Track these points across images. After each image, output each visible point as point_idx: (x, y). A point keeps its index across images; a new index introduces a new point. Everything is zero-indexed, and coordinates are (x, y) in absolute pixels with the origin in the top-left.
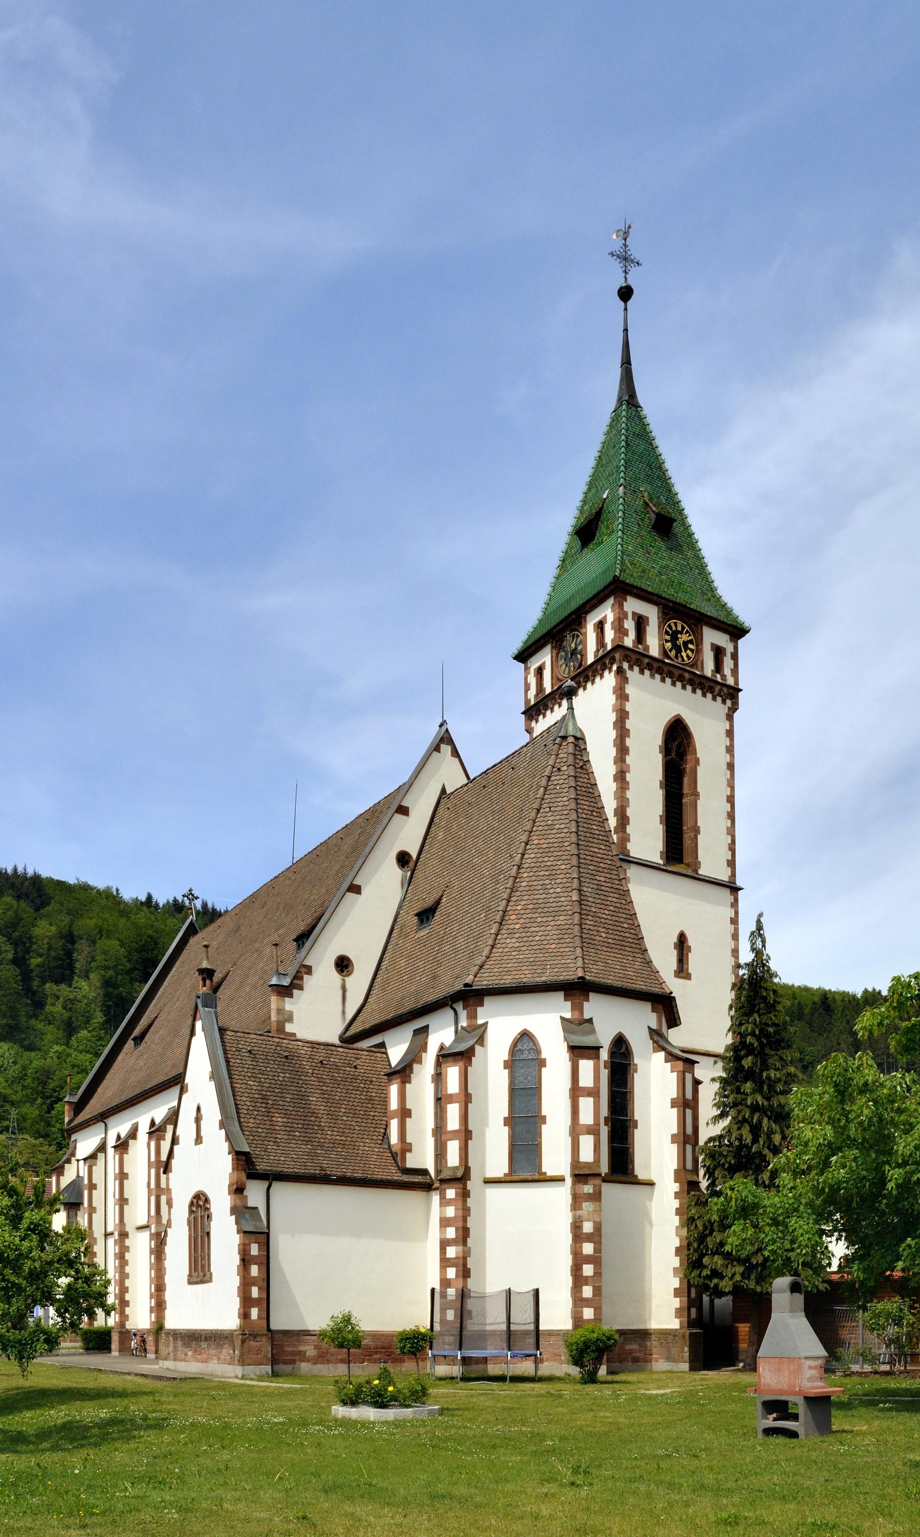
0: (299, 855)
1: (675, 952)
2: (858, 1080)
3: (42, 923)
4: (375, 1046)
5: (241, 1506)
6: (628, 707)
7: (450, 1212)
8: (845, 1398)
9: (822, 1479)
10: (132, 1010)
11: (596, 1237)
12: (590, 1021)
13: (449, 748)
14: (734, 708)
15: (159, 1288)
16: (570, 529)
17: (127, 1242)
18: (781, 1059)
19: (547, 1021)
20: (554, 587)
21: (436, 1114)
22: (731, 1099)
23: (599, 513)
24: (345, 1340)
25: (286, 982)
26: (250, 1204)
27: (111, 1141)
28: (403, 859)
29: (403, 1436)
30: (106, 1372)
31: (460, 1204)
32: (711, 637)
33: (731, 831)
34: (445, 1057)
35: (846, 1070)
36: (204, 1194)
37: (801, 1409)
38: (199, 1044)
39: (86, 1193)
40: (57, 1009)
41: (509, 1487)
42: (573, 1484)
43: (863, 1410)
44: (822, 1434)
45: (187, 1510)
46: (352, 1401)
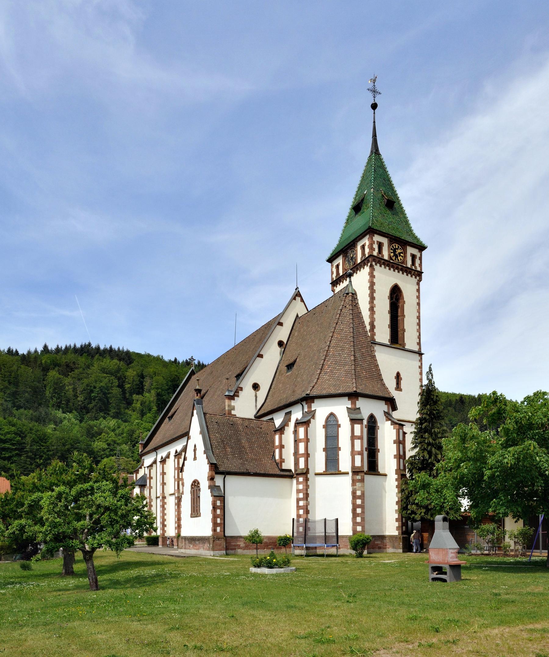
0: (238, 342)
1: (395, 380)
2: (470, 434)
3: (130, 370)
4: (269, 420)
5: (207, 612)
6: (375, 280)
7: (301, 487)
8: (468, 565)
9: (455, 600)
10: (168, 406)
11: (362, 497)
12: (359, 408)
14: (420, 280)
15: (179, 519)
16: (351, 207)
17: (166, 501)
18: (440, 424)
19: (341, 409)
20: (344, 231)
21: (295, 447)
22: (419, 441)
23: (363, 200)
24: (255, 540)
25: (232, 394)
26: (216, 485)
27: (159, 459)
28: (280, 344)
29: (279, 580)
30: (156, 554)
31: (305, 484)
32: (410, 250)
33: (419, 331)
34: (298, 423)
35: (465, 430)
36: (197, 481)
37: (448, 570)
38: (195, 421)
39: (148, 481)
40: (138, 405)
41: (321, 603)
42: (348, 601)
43: (475, 571)
44: (457, 581)
45: (184, 613)
46: (258, 566)
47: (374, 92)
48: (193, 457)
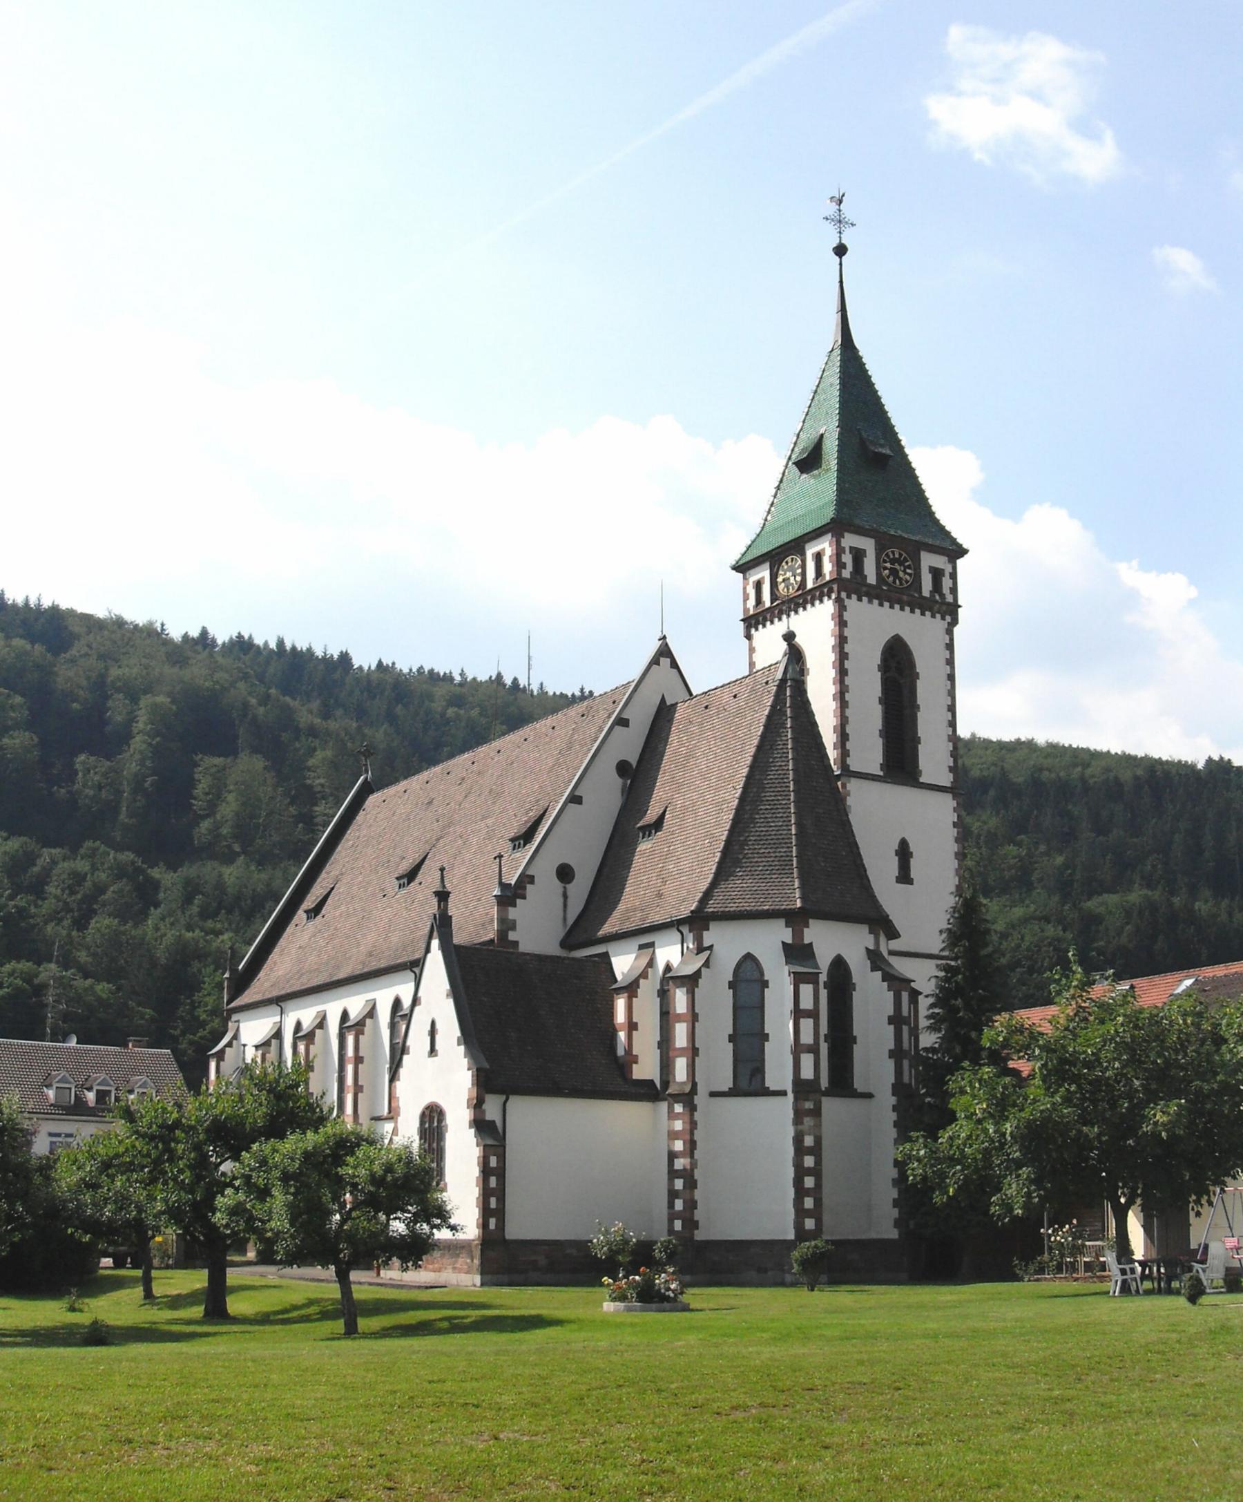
7: (678, 1125)
11: (816, 1151)
13: (668, 660)
14: (955, 622)
19: (766, 942)
31: (687, 1118)
32: (929, 560)
48: (428, 1048)
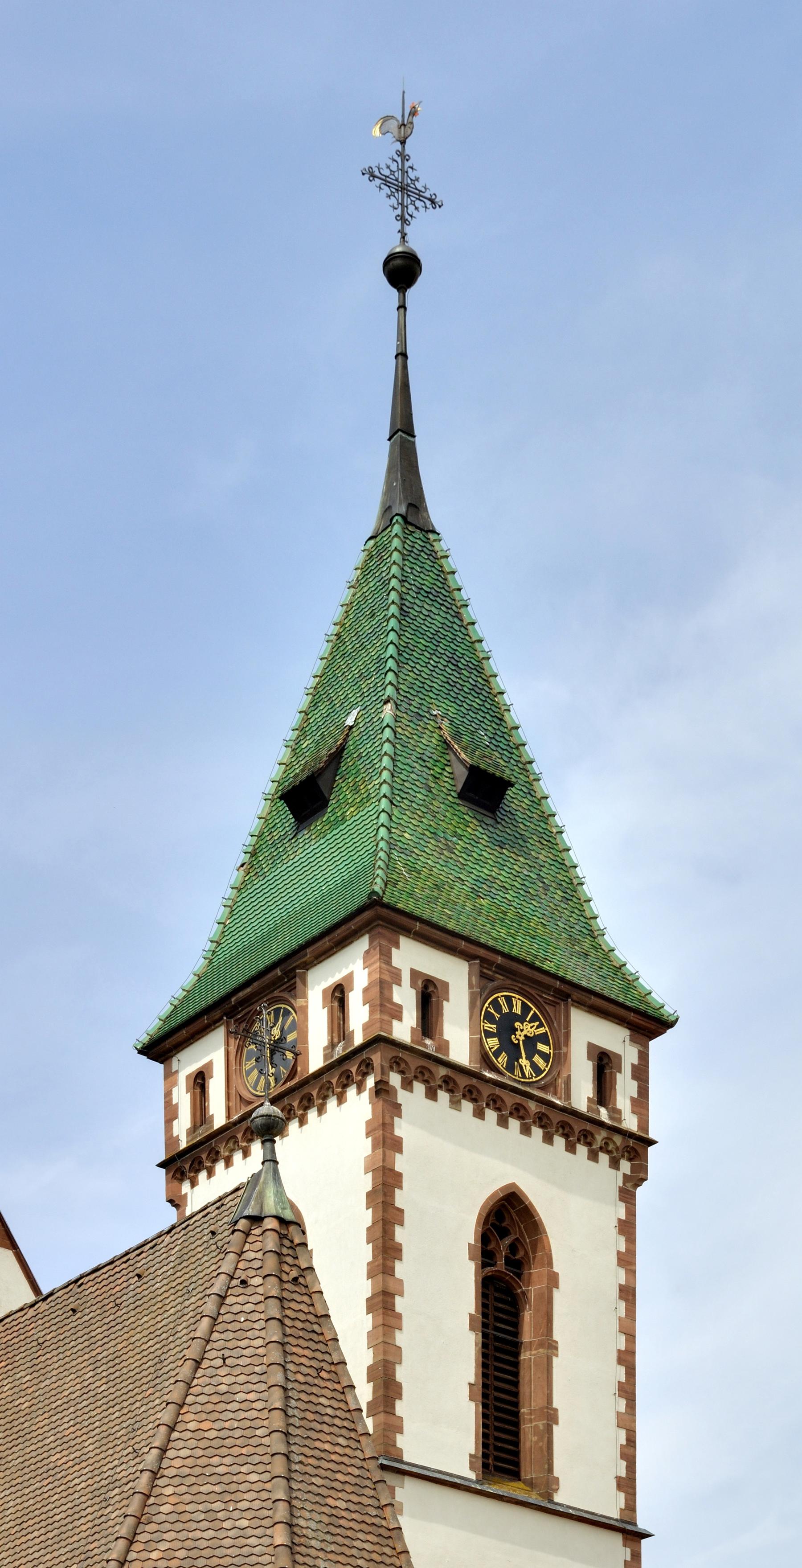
6: (400, 1163)
14: (638, 1177)
16: (271, 788)
20: (232, 909)
23: (337, 756)
32: (587, 1031)
33: (627, 1421)
47: (403, 189)
